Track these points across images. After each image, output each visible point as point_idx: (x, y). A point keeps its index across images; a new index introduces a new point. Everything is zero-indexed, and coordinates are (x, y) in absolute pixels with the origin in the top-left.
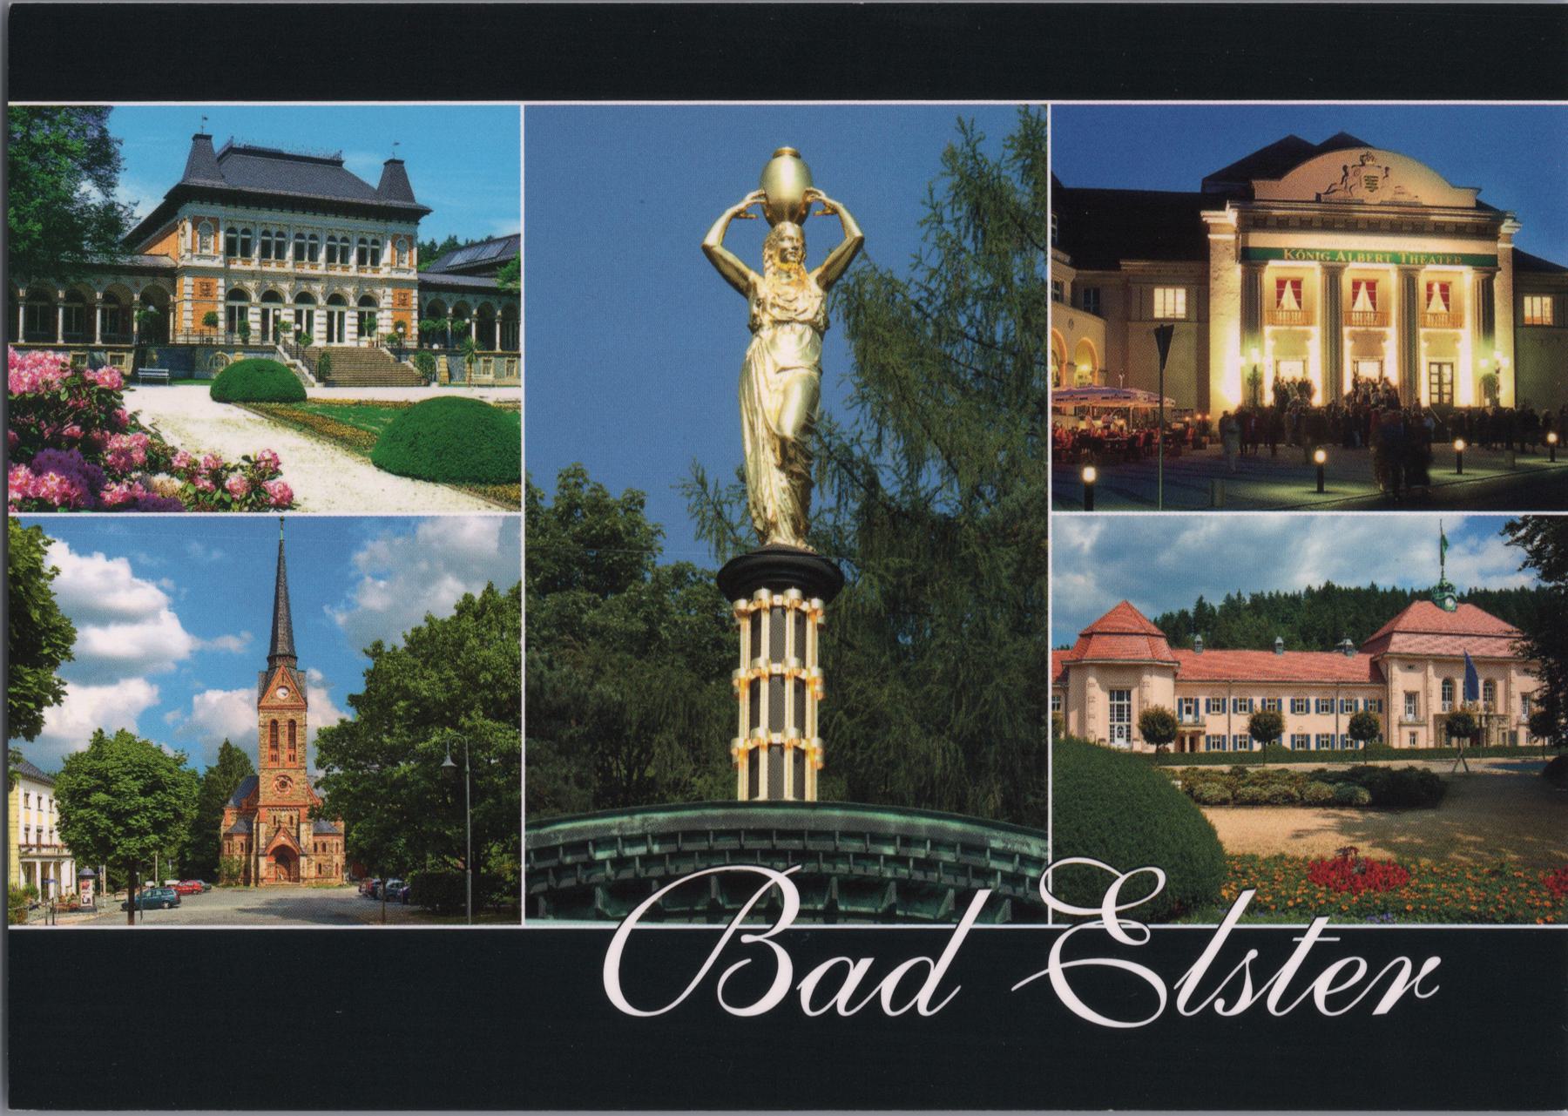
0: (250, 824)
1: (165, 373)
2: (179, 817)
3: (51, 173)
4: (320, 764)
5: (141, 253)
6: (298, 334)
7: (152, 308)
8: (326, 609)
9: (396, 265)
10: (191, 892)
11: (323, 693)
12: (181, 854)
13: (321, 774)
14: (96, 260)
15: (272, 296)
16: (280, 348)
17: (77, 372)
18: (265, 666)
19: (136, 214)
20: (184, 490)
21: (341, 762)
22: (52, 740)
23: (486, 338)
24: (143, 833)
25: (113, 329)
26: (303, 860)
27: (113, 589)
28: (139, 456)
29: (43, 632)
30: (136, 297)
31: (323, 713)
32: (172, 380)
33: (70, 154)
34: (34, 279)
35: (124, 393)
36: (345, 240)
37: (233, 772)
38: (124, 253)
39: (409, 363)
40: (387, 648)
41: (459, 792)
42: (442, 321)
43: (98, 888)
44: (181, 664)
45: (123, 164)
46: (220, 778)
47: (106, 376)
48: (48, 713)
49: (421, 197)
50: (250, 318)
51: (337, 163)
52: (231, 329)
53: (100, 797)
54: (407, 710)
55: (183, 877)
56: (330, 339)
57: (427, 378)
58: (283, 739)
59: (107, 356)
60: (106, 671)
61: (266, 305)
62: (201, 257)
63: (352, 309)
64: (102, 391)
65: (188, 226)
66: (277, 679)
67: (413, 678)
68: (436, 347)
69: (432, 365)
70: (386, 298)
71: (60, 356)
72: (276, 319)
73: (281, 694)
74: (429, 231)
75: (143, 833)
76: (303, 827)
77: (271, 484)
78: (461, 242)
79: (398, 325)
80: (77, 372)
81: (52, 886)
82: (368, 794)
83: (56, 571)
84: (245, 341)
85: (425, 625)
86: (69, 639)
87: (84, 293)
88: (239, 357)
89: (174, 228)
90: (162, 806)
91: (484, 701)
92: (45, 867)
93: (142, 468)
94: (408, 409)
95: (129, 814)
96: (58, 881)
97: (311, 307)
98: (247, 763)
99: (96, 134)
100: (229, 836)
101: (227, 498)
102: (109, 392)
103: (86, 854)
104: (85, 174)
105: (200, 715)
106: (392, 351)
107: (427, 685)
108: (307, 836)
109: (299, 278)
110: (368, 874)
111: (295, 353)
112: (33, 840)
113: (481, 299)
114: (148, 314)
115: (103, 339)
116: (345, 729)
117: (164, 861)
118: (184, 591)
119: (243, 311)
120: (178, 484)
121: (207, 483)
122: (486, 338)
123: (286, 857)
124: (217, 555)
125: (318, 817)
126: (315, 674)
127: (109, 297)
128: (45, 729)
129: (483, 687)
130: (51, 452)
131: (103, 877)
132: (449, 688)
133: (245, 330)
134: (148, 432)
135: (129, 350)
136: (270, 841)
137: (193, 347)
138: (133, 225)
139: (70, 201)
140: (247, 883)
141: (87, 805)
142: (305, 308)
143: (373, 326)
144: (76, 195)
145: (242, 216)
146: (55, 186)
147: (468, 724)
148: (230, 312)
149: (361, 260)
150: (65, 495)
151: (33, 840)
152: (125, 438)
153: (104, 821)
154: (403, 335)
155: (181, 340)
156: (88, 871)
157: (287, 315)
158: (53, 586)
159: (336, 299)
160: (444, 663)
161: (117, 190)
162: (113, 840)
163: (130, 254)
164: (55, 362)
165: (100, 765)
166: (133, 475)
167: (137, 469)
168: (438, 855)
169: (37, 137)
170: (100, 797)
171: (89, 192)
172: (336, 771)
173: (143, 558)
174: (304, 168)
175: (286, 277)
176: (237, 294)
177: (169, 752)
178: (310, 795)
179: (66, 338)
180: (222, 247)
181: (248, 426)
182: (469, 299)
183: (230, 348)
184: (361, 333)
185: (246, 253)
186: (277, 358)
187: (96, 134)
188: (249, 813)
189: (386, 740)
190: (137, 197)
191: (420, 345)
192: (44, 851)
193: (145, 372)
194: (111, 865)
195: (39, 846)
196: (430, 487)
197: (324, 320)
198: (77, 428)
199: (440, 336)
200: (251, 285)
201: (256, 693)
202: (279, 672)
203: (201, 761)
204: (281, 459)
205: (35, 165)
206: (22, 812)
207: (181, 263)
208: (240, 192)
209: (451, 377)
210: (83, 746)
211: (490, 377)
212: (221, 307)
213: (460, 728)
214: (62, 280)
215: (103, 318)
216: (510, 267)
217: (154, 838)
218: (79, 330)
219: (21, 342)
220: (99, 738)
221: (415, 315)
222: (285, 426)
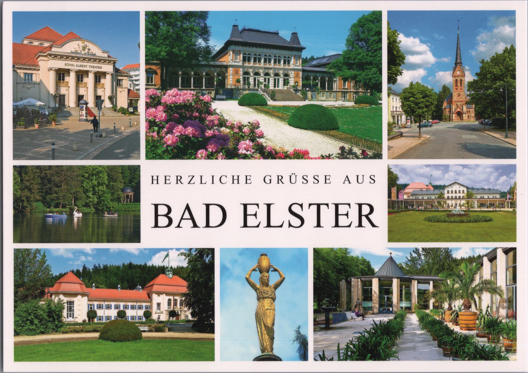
0: (450, 106)
1: (224, 97)
2: (432, 104)
3: (189, 37)
4: (468, 90)
5: (217, 61)
6: (265, 85)
7: (220, 77)
8: (470, 51)
9: (295, 64)
10: (435, 123)
11: (469, 72)
12: (433, 113)
13: (469, 93)
14: (203, 63)
15: (257, 74)
16: (259, 89)
17: (197, 97)
18: (454, 66)
19: (216, 49)
20: (230, 132)
21: (474, 90)
22: (400, 84)
23: (323, 87)
24: (422, 108)
25: (209, 84)
26: (464, 115)
27: (415, 46)
28: (216, 122)
29: (397, 57)
30: (216, 74)
31: (469, 77)
32: (227, 99)
33: (195, 31)
34: (184, 69)
35: (212, 103)
36: (279, 57)
37: (446, 93)
38: (211, 61)
39: (299, 94)
40: (485, 61)
41: (504, 98)
42: (309, 81)
43: (411, 122)
44: (433, 65)
45: (211, 34)
46: (443, 94)
47: (206, 98)
48: (399, 78)
49: (303, 44)
50: (250, 80)
51: (277, 34)
52: (244, 84)
53: (412, 99)
54: (491, 77)
55: (433, 119)
56: (275, 87)
57: (305, 98)
58: (459, 84)
59: (206, 92)
60: (413, 67)
61: (255, 76)
62: (235, 62)
63: (282, 78)
64: (205, 102)
65: (231, 53)
66: (457, 69)
67: (492, 68)
68: (307, 89)
69: (306, 95)
70: (292, 74)
71: (192, 92)
72: (258, 81)
73: (458, 73)
74: (305, 54)
75: (422, 108)
76: (464, 106)
77: (257, 130)
78: (315, 57)
79: (296, 82)
80: (197, 97)
81: (399, 122)
82: (480, 98)
83: (400, 41)
84: (249, 87)
85: (495, 55)
86: (404, 59)
87: (200, 73)
88: (247, 92)
89: (227, 53)
90: (428, 101)
91: (510, 74)
92: (398, 117)
93: (217, 125)
94: (299, 108)
95: (419, 103)
96: (401, 120)
97: (269, 77)
98: (449, 90)
99: (203, 25)
100: (445, 109)
101: (243, 135)
102: (207, 103)
103: (408, 114)
104: (200, 37)
105: (437, 78)
106: (294, 90)
107: (496, 70)
108: (465, 109)
109: (265, 68)
110: (481, 118)
111: (264, 91)
112: (395, 110)
113: (321, 75)
114: (219, 79)
115: (205, 87)
116: (475, 82)
117: (428, 116)
118: (433, 46)
119: (248, 78)
120: (228, 130)
121: (237, 130)
122: (323, 87)
123: (460, 114)
124: (442, 37)
125: (468, 104)
126: (467, 68)
127: (207, 74)
128: (398, 82)
129: (510, 71)
130: (189, 121)
131: (413, 119)
132: (501, 71)
133: (249, 84)
134: (219, 115)
135: (213, 90)
136: (456, 110)
137: (232, 89)
138: (213, 54)
139: (195, 45)
140: (450, 121)
141: (409, 101)
142: (267, 77)
143: (288, 83)
144: (197, 43)
145: (248, 49)
146: (191, 41)
147: (507, 80)
148: (244, 79)
149: (285, 63)
150: (194, 134)
151: (395, 110)
152: (212, 117)
153: (413, 105)
154: (297, 85)
155: (229, 87)
156: (409, 118)
157: (262, 80)
158: (399, 45)
159: (277, 75)
160: (500, 65)
161: (209, 42)
162: (415, 110)
163: (214, 61)
164: (191, 94)
165: (411, 90)
166: (215, 128)
167: (216, 126)
168: (499, 113)
169: (185, 26)
170: (412, 99)
171: (201, 42)
172: (473, 92)
173: (423, 38)
174: (266, 35)
175: (261, 68)
176: (246, 73)
177: (430, 87)
178: (466, 98)
179: (194, 87)
180: (241, 59)
181: (250, 113)
182: (318, 75)
183: (244, 89)
184: (284, 85)
185: (249, 61)
186: (258, 93)
187: (203, 25)
188: (450, 102)
189: (485, 84)
190: (216, 44)
191: (303, 88)
192: (398, 113)
193: (218, 97)
194: (415, 116)
195: (396, 111)
196: (306, 131)
197: (273, 81)
198: (197, 114)
199: (309, 86)
200: (251, 70)
201: (452, 72)
202: (458, 67)
203: (438, 90)
204: (260, 123)
205: (184, 34)
206: (392, 103)
207: (229, 64)
208: (247, 42)
209: (312, 98)
210: (407, 86)
211: (324, 98)
212: (241, 77)
213: (504, 81)
214: (193, 69)
215: (205, 81)
216: (330, 65)
217: (425, 109)
218: (198, 84)
219: (180, 88)
220: (411, 84)
221: (301, 79)
222: (261, 113)
